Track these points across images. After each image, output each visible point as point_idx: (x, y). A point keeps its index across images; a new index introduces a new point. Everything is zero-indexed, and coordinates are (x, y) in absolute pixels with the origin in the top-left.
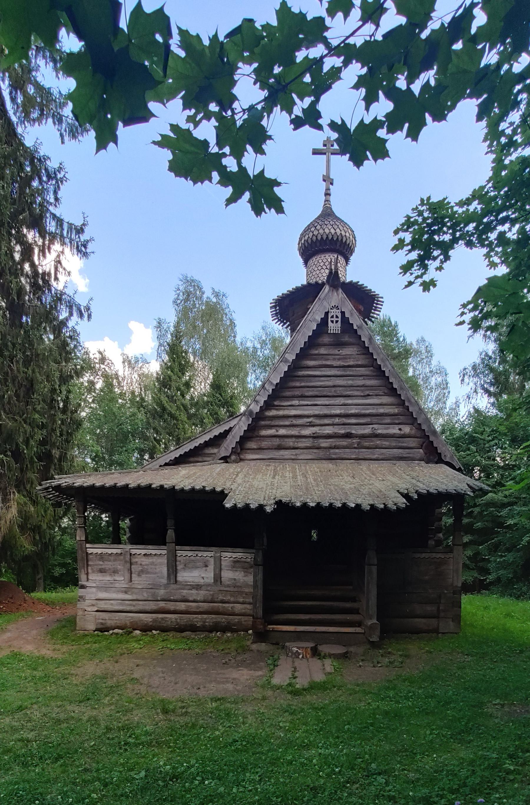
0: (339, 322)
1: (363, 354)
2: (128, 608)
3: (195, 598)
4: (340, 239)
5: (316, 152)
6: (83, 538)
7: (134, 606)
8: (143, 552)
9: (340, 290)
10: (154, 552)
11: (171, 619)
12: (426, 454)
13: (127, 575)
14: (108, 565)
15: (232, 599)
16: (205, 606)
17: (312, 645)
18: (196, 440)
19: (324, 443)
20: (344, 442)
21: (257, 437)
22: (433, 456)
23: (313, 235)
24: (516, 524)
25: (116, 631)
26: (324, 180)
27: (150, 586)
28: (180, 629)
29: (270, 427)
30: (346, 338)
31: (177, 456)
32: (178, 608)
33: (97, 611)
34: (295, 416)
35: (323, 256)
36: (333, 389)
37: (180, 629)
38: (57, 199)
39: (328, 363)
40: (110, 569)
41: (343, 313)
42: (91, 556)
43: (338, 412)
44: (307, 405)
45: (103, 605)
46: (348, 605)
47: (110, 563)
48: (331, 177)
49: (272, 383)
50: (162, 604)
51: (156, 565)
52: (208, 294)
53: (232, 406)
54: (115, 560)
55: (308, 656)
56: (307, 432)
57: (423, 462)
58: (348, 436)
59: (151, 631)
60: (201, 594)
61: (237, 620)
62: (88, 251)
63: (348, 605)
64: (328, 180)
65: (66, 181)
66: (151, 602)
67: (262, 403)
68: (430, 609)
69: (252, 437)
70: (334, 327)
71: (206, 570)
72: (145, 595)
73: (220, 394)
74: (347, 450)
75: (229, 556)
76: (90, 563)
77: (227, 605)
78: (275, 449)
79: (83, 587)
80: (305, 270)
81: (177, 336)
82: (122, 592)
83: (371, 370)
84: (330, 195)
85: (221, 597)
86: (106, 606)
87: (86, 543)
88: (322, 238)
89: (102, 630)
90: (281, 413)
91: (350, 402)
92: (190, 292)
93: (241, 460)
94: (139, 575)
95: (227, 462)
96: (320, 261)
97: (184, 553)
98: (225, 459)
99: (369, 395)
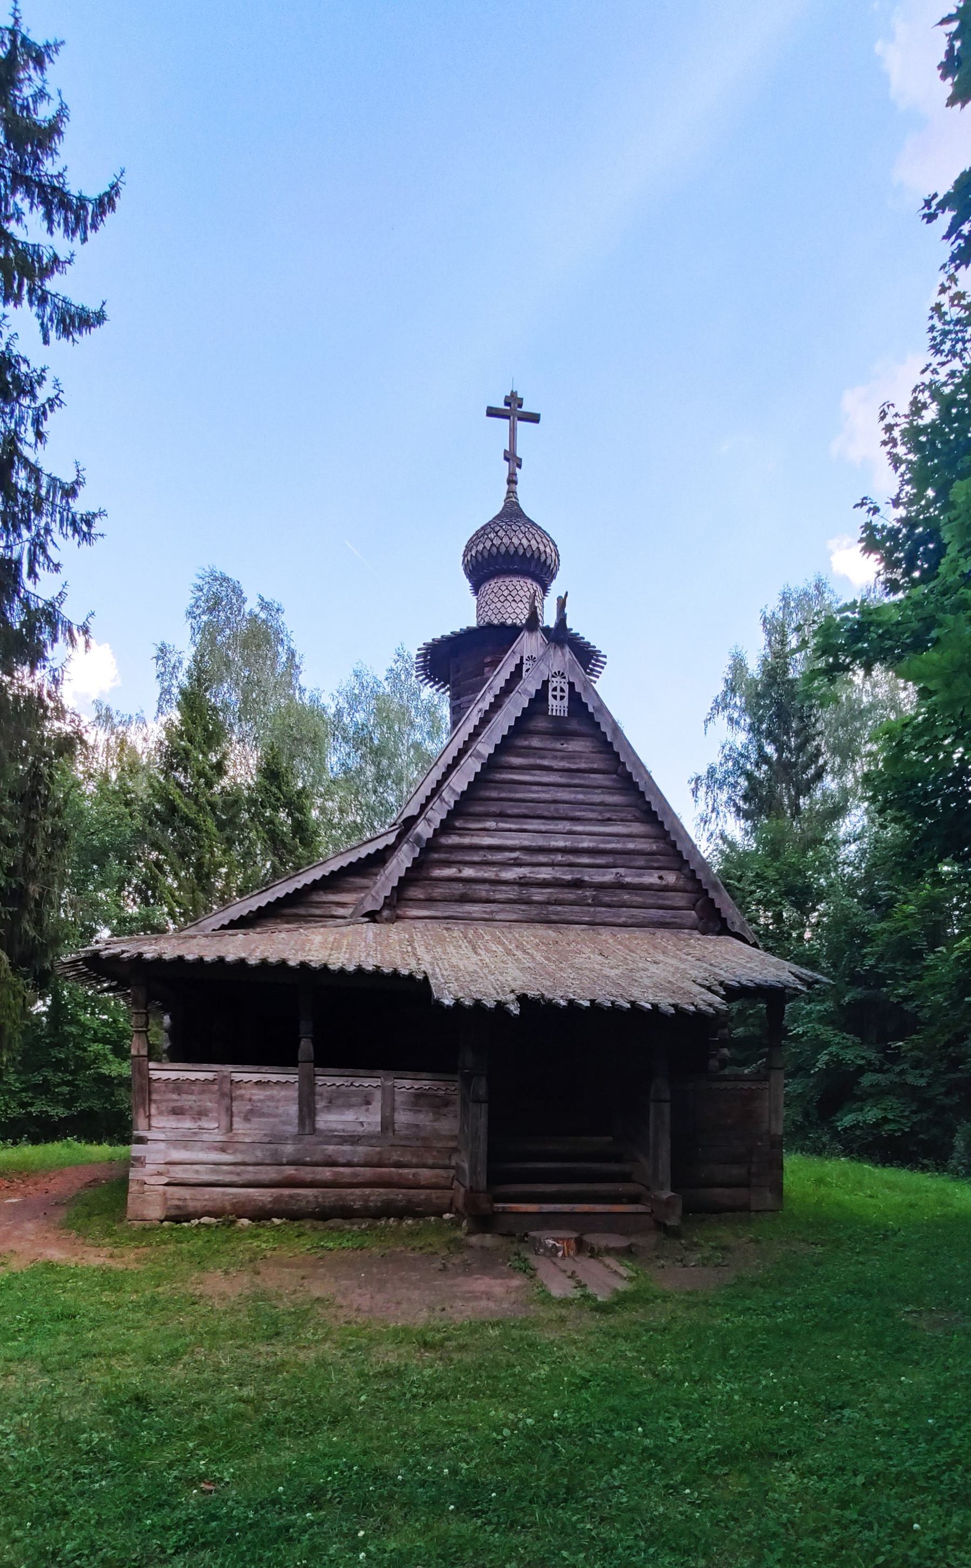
0: (566, 699)
1: (600, 752)
2: (228, 1178)
3: (349, 1158)
4: (536, 556)
5: (492, 412)
6: (144, 1052)
7: (238, 1174)
8: (255, 1077)
9: (567, 649)
10: (274, 1078)
11: (306, 1196)
12: (701, 918)
13: (224, 1121)
14: (188, 1100)
15: (415, 1160)
16: (367, 1173)
17: (575, 1235)
18: (297, 878)
19: (539, 895)
20: (570, 895)
21: (426, 879)
22: (714, 923)
23: (493, 545)
24: (805, 1033)
25: (205, 1220)
26: (506, 459)
27: (267, 1140)
28: (322, 1214)
29: (448, 864)
30: (574, 725)
31: (263, 904)
32: (318, 1177)
33: (166, 1185)
34: (490, 848)
35: (507, 580)
36: (553, 806)
37: (322, 1214)
38: (39, 435)
39: (546, 762)
40: (191, 1107)
41: (571, 685)
42: (156, 1085)
43: (561, 844)
44: (510, 830)
45: (179, 1173)
46: (615, 1167)
47: (194, 1098)
48: (518, 455)
49: (454, 791)
50: (290, 1171)
51: (278, 1101)
52: (251, 605)
53: (301, 809)
54: (203, 1092)
55: (572, 1253)
56: (510, 874)
57: (696, 932)
58: (577, 884)
59: (269, 1219)
60: (362, 1150)
61: (423, 1197)
62: (93, 531)
63: (615, 1167)
64: (512, 458)
65: (60, 406)
66: (269, 1168)
67: (437, 824)
68: (736, 1171)
69: (418, 880)
70: (557, 706)
71: (367, 1110)
72: (259, 1153)
73: (279, 788)
74: (576, 908)
75: (406, 1085)
76: (154, 1097)
77: (406, 1171)
78: (456, 901)
79: (141, 1140)
80: (474, 600)
81: (202, 678)
82: (216, 1149)
83: (614, 780)
84: (516, 483)
85: (395, 1157)
86: (185, 1176)
87: (150, 1060)
88: (507, 551)
89: (177, 1219)
90: (467, 841)
91: (579, 828)
92: (217, 599)
93: (399, 918)
94: (247, 1119)
95: (375, 921)
96: (503, 588)
97: (327, 1081)
98: (373, 916)
99: (609, 819)
